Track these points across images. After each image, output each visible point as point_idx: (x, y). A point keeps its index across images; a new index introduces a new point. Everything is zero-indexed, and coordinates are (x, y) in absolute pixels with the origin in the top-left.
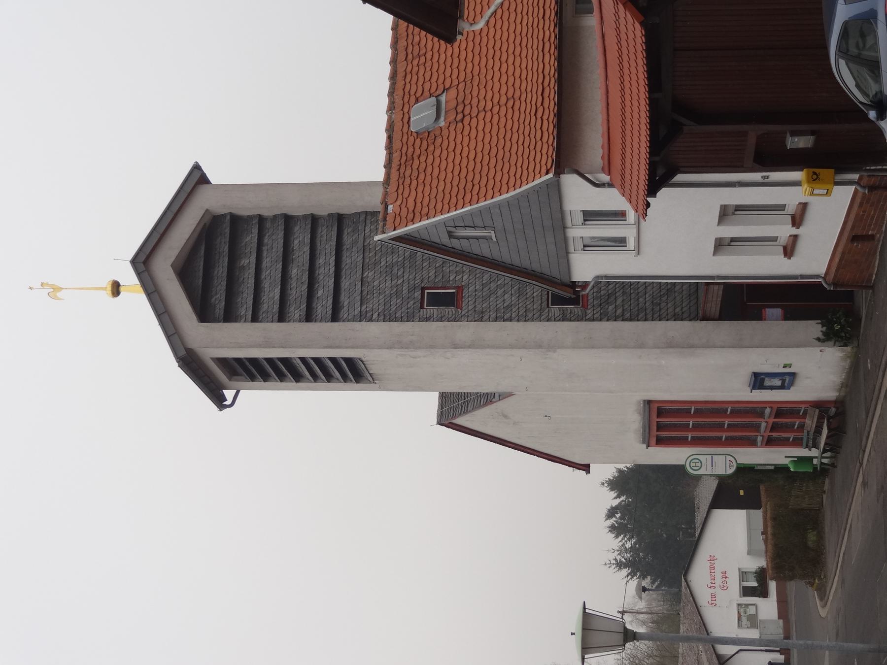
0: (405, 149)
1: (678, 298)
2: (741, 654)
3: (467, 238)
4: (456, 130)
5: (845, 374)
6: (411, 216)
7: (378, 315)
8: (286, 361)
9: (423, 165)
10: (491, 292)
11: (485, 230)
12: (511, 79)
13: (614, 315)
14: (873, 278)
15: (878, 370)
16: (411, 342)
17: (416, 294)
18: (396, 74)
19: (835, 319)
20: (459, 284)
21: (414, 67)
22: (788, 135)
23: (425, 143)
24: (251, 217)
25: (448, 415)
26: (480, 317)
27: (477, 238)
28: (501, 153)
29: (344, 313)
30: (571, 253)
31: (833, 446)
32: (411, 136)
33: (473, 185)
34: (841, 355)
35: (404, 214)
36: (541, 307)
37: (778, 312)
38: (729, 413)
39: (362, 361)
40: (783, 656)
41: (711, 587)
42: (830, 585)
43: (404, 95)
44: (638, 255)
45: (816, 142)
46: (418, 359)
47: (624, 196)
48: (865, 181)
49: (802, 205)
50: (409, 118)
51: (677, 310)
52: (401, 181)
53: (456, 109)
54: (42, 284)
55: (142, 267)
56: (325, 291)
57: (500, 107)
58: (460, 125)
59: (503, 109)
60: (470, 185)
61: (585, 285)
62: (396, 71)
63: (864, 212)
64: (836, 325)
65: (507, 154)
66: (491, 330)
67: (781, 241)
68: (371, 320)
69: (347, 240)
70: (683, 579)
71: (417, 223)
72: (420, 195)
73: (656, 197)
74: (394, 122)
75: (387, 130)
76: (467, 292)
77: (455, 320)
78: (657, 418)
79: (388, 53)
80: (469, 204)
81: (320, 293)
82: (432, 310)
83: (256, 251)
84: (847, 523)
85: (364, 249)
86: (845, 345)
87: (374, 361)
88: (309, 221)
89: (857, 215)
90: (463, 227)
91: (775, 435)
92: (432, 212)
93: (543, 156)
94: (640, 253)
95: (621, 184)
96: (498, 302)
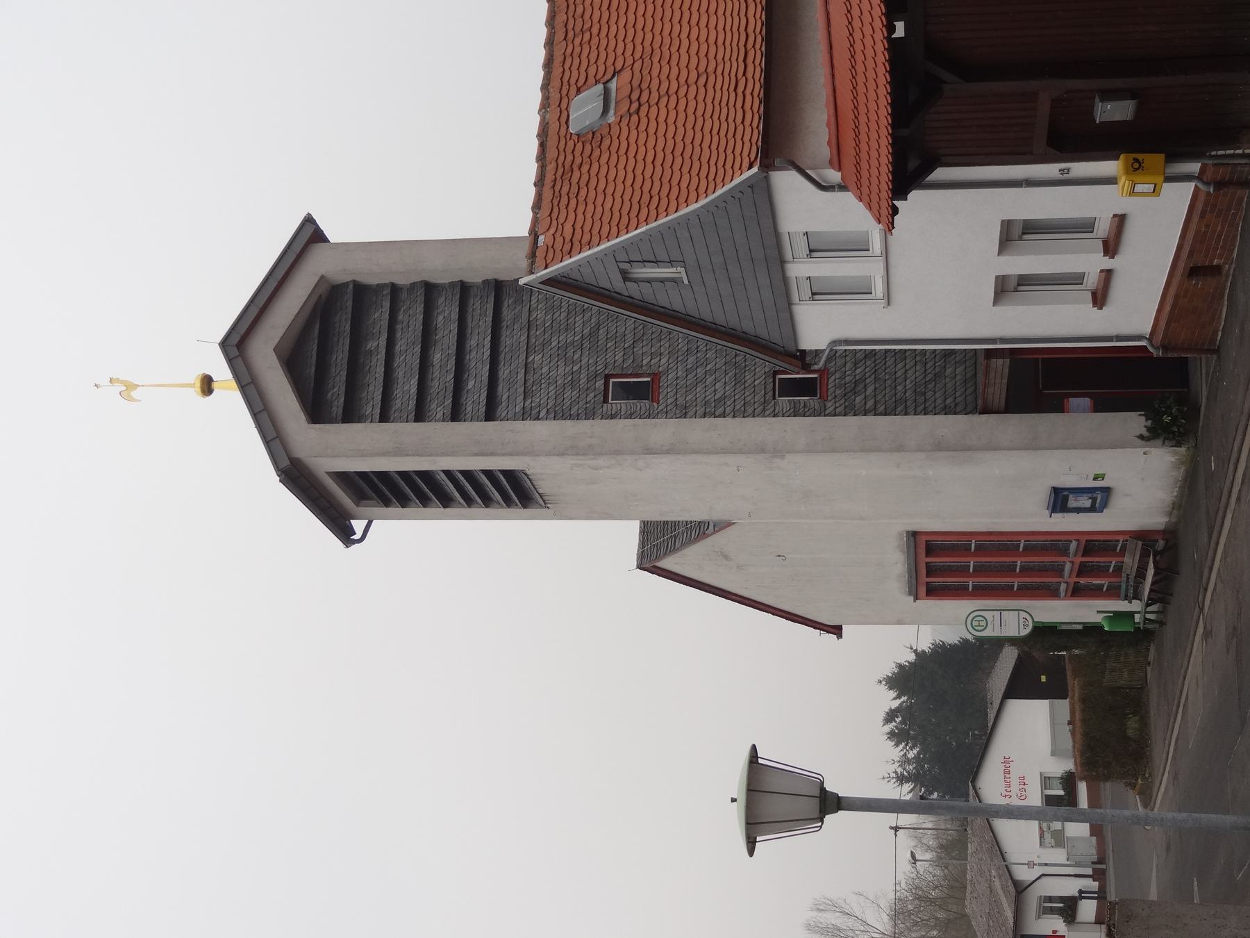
0: (562, 158)
1: (949, 385)
2: (1044, 880)
3: (649, 281)
4: (630, 125)
5: (1177, 489)
6: (567, 247)
7: (547, 412)
8: (426, 476)
9: (585, 178)
10: (698, 381)
11: (672, 266)
12: (704, 48)
13: (863, 408)
14: (1219, 338)
15: (1226, 465)
16: (590, 446)
17: (598, 384)
18: (552, 60)
19: (1163, 409)
20: (654, 369)
21: (575, 48)
22: (1097, 99)
23: (588, 147)
24: (381, 287)
25: (651, 556)
26: (684, 412)
27: (662, 281)
28: (689, 148)
29: (501, 410)
30: (796, 304)
31: (1161, 594)
32: (570, 139)
33: (651, 197)
34: (1173, 459)
35: (558, 245)
36: (765, 399)
37: (1086, 402)
38: (1021, 549)
39: (526, 474)
40: (1097, 883)
41: (1006, 796)
42: (1157, 785)
43: (562, 85)
44: (889, 304)
45: (1138, 112)
46: (601, 472)
47: (861, 201)
48: (1209, 175)
49: (1117, 219)
50: (568, 116)
51: (948, 401)
52: (555, 203)
53: (629, 97)
54: (111, 380)
55: (235, 352)
56: (476, 384)
57: (688, 87)
58: (635, 118)
59: (693, 89)
60: (646, 197)
61: (817, 353)
62: (552, 56)
63: (1208, 226)
64: (1165, 416)
65: (697, 149)
66: (697, 429)
67: (1088, 286)
68: (537, 418)
69: (507, 314)
70: (971, 787)
71: (576, 255)
72: (580, 217)
73: (906, 200)
74: (548, 123)
75: (539, 135)
76: (665, 381)
77: (649, 417)
78: (926, 557)
79: (543, 32)
80: (645, 223)
81: (471, 384)
82: (619, 405)
83: (387, 330)
84: (1180, 698)
85: (529, 326)
86: (1178, 445)
87: (542, 474)
88: (458, 290)
89: (1197, 232)
90: (640, 262)
91: (1082, 581)
92: (596, 239)
93: (745, 145)
94: (891, 303)
95: (853, 183)
96: (707, 394)
